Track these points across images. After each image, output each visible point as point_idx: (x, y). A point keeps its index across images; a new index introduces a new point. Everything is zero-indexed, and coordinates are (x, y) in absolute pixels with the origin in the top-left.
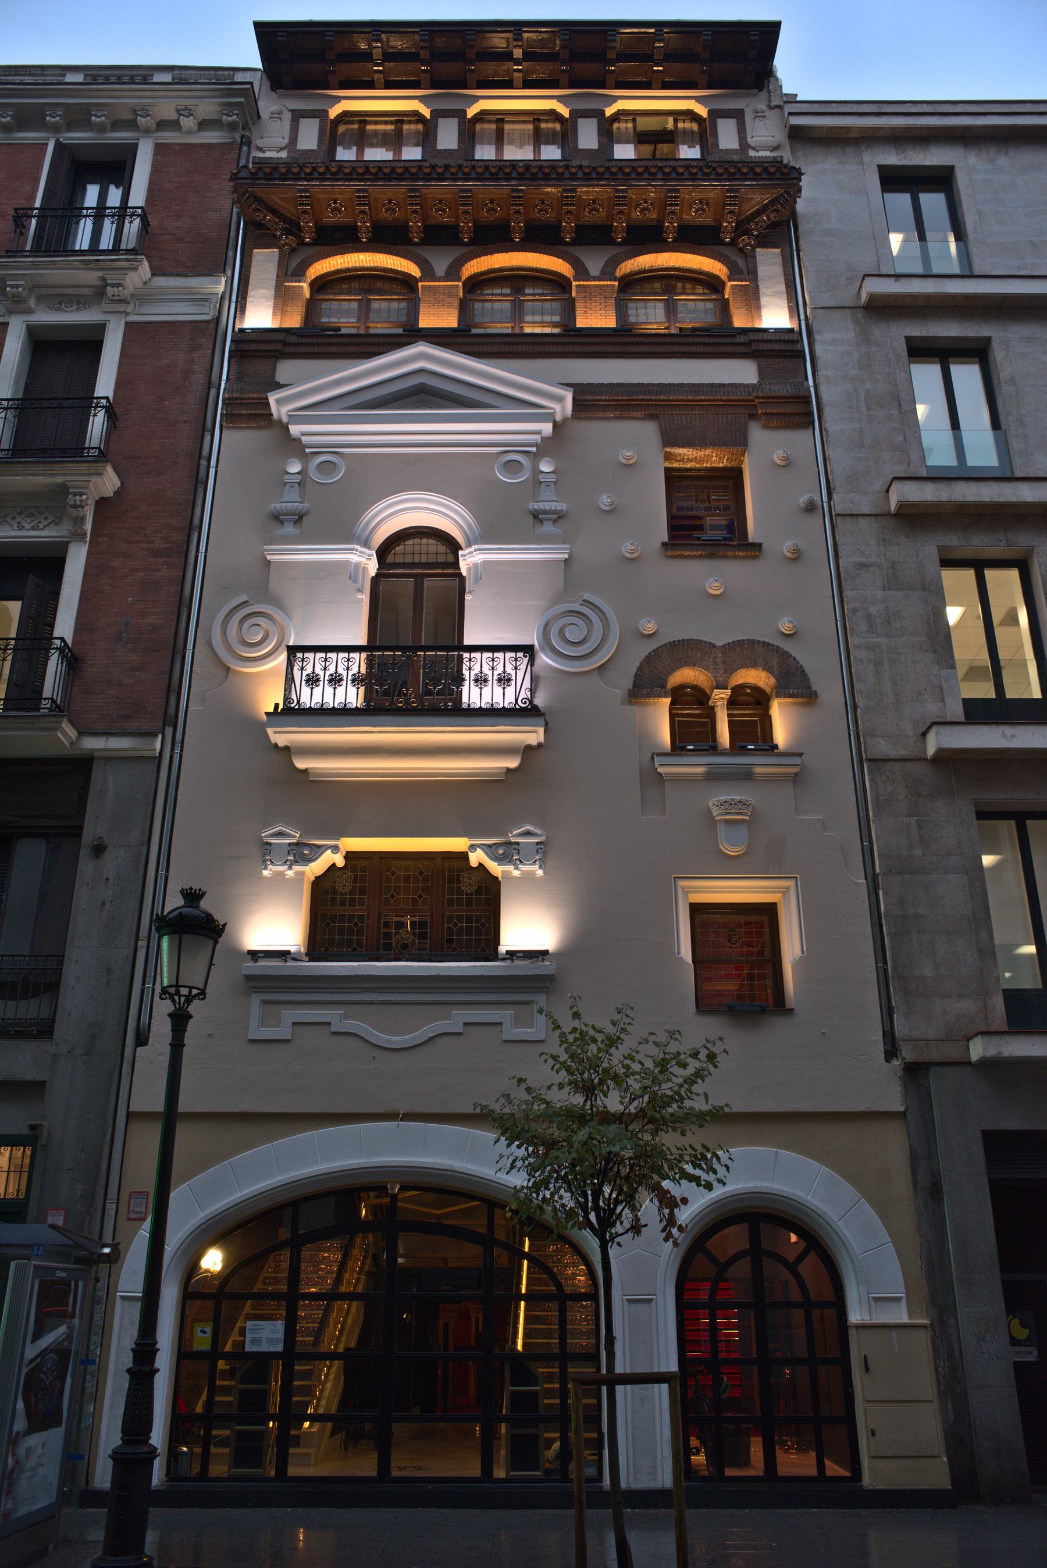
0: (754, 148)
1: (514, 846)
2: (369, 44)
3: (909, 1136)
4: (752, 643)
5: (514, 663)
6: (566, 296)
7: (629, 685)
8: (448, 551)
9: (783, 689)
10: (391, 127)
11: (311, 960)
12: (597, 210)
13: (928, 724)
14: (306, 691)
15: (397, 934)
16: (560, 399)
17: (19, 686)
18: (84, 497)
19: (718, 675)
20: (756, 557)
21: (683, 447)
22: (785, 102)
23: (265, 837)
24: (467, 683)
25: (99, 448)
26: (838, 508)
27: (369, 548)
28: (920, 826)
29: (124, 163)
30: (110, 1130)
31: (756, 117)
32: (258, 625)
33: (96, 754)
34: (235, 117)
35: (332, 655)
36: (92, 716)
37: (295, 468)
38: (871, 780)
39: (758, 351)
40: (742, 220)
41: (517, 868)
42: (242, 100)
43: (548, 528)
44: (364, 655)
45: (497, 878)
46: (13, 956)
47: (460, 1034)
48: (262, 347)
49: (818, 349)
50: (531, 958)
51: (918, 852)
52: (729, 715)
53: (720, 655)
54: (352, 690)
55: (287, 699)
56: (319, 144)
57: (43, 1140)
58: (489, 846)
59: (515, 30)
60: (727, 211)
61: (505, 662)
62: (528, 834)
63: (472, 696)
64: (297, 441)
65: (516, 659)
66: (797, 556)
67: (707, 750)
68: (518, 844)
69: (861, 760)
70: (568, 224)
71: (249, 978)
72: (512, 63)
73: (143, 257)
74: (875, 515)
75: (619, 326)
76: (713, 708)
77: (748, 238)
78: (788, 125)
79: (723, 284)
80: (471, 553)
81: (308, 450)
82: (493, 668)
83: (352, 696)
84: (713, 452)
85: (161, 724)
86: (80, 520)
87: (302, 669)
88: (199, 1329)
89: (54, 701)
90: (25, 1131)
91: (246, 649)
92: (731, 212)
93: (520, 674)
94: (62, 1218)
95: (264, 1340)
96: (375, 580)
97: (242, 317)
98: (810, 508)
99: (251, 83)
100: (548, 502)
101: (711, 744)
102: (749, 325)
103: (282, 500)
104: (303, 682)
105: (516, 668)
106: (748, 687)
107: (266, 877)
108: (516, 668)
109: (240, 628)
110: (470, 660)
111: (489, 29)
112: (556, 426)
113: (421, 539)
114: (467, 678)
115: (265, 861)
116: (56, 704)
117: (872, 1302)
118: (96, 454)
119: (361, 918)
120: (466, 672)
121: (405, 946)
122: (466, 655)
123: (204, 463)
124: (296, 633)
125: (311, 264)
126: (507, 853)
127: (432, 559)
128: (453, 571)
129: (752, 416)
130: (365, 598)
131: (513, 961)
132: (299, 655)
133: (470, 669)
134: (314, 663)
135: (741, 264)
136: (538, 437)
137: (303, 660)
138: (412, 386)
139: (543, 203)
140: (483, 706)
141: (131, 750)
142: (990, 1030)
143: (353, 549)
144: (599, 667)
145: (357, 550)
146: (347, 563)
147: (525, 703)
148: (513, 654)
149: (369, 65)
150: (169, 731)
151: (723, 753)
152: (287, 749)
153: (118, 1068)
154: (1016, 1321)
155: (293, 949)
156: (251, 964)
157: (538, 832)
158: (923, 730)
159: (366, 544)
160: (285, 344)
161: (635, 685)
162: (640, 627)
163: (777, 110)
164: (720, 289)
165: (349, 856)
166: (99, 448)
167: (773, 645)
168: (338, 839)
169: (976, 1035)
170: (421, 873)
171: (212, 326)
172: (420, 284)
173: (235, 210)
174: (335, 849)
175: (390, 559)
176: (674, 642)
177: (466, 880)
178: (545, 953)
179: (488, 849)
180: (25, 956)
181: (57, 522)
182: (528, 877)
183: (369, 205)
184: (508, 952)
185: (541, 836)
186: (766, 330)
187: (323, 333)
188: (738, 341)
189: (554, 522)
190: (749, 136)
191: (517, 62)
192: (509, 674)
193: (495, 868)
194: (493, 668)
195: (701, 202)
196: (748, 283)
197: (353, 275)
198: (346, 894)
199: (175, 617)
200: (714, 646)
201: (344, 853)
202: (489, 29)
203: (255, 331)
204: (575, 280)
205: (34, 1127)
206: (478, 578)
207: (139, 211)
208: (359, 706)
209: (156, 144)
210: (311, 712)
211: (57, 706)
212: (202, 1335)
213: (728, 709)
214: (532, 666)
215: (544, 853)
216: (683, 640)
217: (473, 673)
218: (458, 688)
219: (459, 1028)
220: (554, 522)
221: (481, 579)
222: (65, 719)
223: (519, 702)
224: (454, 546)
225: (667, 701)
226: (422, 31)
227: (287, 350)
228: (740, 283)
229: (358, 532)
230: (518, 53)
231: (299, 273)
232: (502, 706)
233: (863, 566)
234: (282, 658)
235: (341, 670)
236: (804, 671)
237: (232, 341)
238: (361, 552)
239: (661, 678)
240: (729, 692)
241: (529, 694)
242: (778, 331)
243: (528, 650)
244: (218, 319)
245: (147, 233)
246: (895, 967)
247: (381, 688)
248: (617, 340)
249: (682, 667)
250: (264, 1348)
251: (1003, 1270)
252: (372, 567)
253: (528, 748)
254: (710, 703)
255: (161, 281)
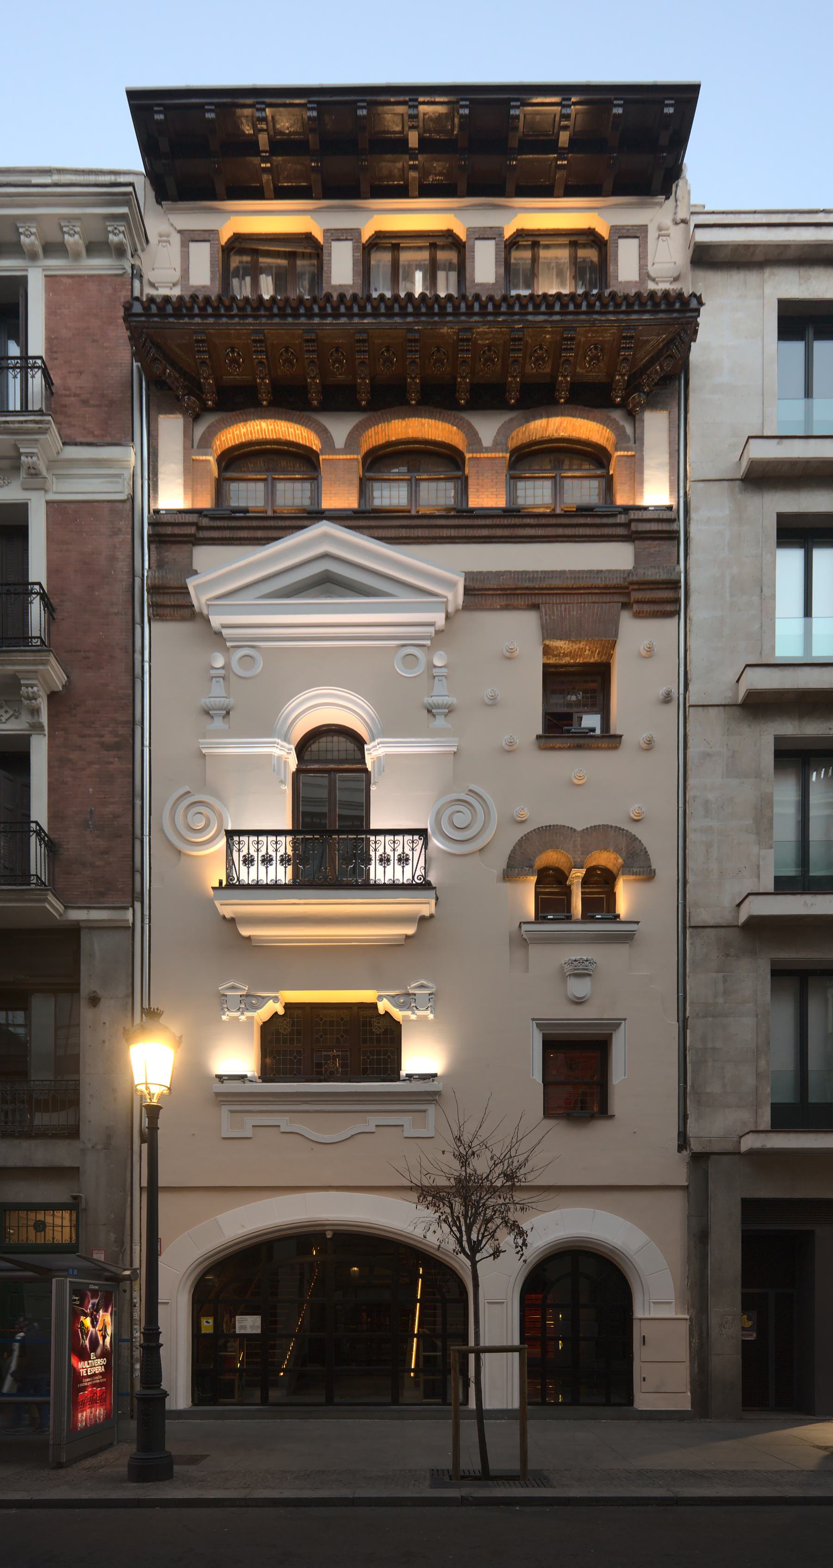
0: (653, 280)
1: (412, 997)
2: (254, 127)
3: (688, 1201)
4: (606, 828)
5: (411, 845)
6: (459, 473)
7: (504, 865)
8: (356, 749)
9: (627, 868)
10: (283, 262)
11: (264, 1081)
12: (492, 361)
13: (745, 894)
14: (243, 869)
15: (326, 1064)
16: (451, 585)
17: (7, 868)
18: (35, 689)
19: (576, 856)
20: (616, 748)
21: (561, 639)
22: (692, 213)
23: (222, 990)
24: (373, 862)
25: (40, 638)
26: (693, 699)
27: (289, 743)
28: (725, 980)
29: (17, 305)
30: (129, 1199)
31: (659, 236)
32: (201, 813)
33: (82, 924)
34: (121, 236)
35: (263, 839)
36: (74, 893)
37: (219, 661)
38: (692, 944)
39: (637, 532)
40: (635, 373)
41: (413, 1013)
42: (124, 210)
43: (440, 722)
44: (289, 838)
45: (399, 1022)
46: (42, 1081)
47: (374, 1133)
48: (177, 530)
49: (693, 529)
50: (424, 1079)
51: (721, 1000)
52: (583, 893)
53: (579, 839)
54: (281, 869)
55: (229, 876)
56: (212, 279)
57: (83, 1205)
58: (393, 997)
59: (411, 100)
60: (621, 358)
61: (404, 844)
62: (422, 986)
63: (378, 873)
64: (219, 634)
65: (413, 842)
66: (649, 745)
67: (563, 919)
68: (415, 994)
69: (685, 928)
70: (464, 381)
71: (218, 1094)
72: (407, 157)
73: (49, 418)
74: (724, 706)
75: (508, 506)
76: (569, 887)
77: (639, 396)
78: (692, 244)
79: (609, 457)
80: (375, 746)
81: (229, 644)
82: (394, 850)
83: (282, 874)
84: (586, 645)
85: (130, 900)
86: (35, 712)
87: (239, 850)
88: (205, 1321)
89: (39, 878)
90: (70, 1201)
91: (199, 835)
92: (625, 359)
93: (416, 854)
94: (103, 1255)
95: (248, 1326)
96: (296, 775)
97: (156, 498)
98: (667, 699)
99: (131, 184)
100: (441, 695)
101: (566, 914)
102: (630, 503)
103: (210, 695)
104: (241, 862)
105: (413, 849)
106: (600, 869)
107: (224, 1021)
108: (413, 849)
109: (186, 816)
110: (375, 842)
111: (382, 98)
112: (447, 617)
113: (333, 737)
114: (373, 858)
115: (222, 1009)
116: (40, 879)
117: (652, 1304)
118: (39, 643)
119: (299, 1052)
120: (372, 853)
121: (332, 1073)
122: (372, 838)
123: (138, 656)
124: (232, 821)
125: (215, 434)
126: (407, 1001)
127: (343, 756)
128: (359, 766)
129: (625, 606)
130: (288, 788)
131: (411, 1081)
132: (236, 838)
133: (375, 850)
134: (248, 845)
135: (629, 430)
136: (431, 630)
137: (239, 843)
138: (317, 574)
139: (438, 351)
140: (386, 882)
141: (109, 920)
142: (758, 1129)
143: (275, 743)
144: (481, 850)
145: (278, 744)
146: (270, 756)
147: (420, 879)
148: (410, 837)
149: (256, 160)
150: (138, 905)
151: (576, 922)
152: (232, 920)
153: (129, 1160)
154: (745, 1316)
155: (249, 1074)
156: (220, 1085)
157: (430, 985)
158: (738, 902)
159: (286, 739)
160: (200, 528)
161: (509, 866)
162: (515, 814)
163: (682, 225)
164: (605, 462)
165: (288, 1006)
166: (40, 638)
167: (623, 830)
168: (277, 991)
169: (748, 1133)
170: (342, 1019)
171: (128, 506)
172: (321, 457)
173: (135, 364)
174: (276, 999)
175: (307, 756)
176: (542, 827)
177: (376, 1024)
178: (435, 1075)
179: (391, 998)
180: (51, 1081)
181: (16, 716)
182: (422, 1020)
183: (265, 352)
184: (407, 1075)
185: (433, 988)
186: (645, 508)
187: (233, 515)
188: (618, 521)
189: (446, 716)
190: (650, 264)
191: (413, 154)
192: (407, 855)
193: (398, 1014)
194: (394, 850)
195: (596, 348)
196: (633, 453)
197: (256, 450)
198: (287, 1035)
199: (130, 806)
200: (575, 830)
201: (284, 1004)
202: (382, 98)
203: (169, 512)
204: (469, 451)
205: (75, 1198)
206: (381, 770)
207: (39, 362)
208: (287, 882)
209: (46, 276)
210: (248, 887)
211: (43, 883)
212: (207, 1324)
213: (582, 888)
214: (426, 849)
215: (434, 1001)
216: (550, 826)
217: (378, 854)
218: (366, 867)
219: (373, 1129)
220: (446, 716)
221: (384, 771)
222: (49, 892)
223: (416, 878)
224: (358, 741)
225: (534, 879)
226: (310, 102)
227: (202, 534)
228: (626, 453)
229: (278, 727)
230: (413, 139)
231: (205, 443)
232: (401, 882)
233: (707, 755)
234: (222, 842)
235: (271, 852)
236: (647, 852)
237: (149, 524)
238: (282, 746)
239: (530, 860)
240: (584, 871)
241: (423, 871)
242: (658, 508)
243: (422, 833)
244: (133, 498)
245: (52, 393)
246: (693, 1086)
247: (304, 867)
248: (506, 521)
249: (548, 849)
250: (249, 1331)
251: (744, 1284)
252: (293, 763)
253: (423, 920)
254: (568, 883)
255: (72, 452)
